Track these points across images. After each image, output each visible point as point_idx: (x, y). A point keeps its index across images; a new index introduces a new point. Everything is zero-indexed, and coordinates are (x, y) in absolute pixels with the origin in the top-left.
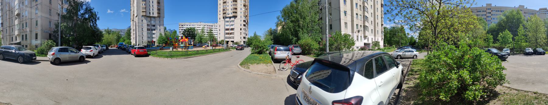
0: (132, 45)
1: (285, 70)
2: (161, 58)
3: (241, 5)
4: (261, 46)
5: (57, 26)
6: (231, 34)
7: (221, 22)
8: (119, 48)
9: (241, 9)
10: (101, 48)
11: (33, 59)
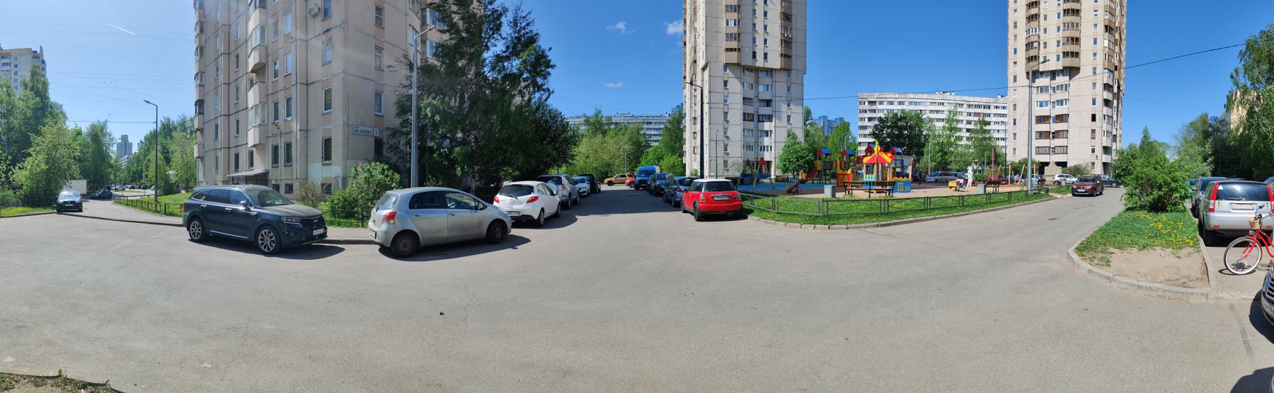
0: (688, 174)
1: (1247, 271)
2: (789, 224)
3: (1095, 25)
4: (1162, 181)
5: (403, 109)
6: (1056, 134)
7: (1019, 90)
8: (637, 187)
9: (1095, 43)
10: (568, 187)
11: (313, 238)
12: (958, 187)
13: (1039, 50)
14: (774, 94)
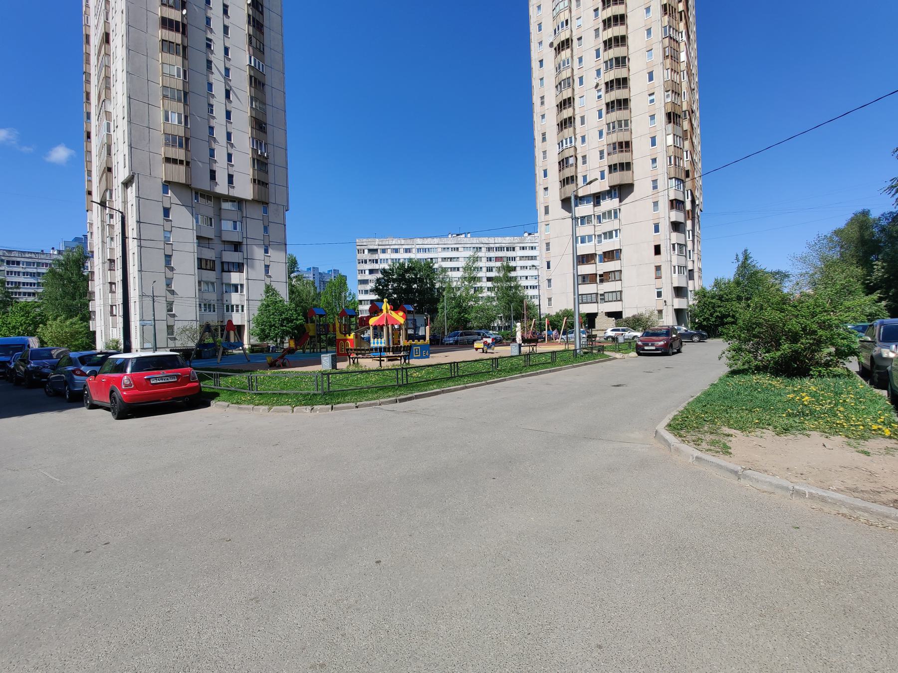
0: (100, 346)
2: (274, 408)
6: (605, 277)
9: (653, 144)
12: (485, 348)
13: (576, 167)
14: (245, 236)
